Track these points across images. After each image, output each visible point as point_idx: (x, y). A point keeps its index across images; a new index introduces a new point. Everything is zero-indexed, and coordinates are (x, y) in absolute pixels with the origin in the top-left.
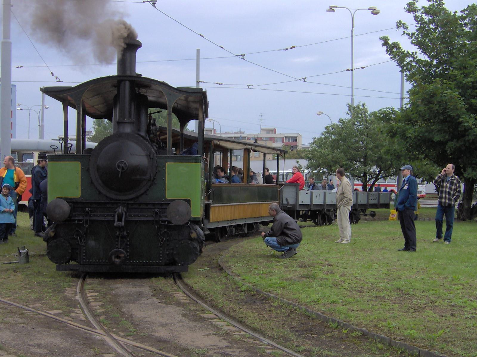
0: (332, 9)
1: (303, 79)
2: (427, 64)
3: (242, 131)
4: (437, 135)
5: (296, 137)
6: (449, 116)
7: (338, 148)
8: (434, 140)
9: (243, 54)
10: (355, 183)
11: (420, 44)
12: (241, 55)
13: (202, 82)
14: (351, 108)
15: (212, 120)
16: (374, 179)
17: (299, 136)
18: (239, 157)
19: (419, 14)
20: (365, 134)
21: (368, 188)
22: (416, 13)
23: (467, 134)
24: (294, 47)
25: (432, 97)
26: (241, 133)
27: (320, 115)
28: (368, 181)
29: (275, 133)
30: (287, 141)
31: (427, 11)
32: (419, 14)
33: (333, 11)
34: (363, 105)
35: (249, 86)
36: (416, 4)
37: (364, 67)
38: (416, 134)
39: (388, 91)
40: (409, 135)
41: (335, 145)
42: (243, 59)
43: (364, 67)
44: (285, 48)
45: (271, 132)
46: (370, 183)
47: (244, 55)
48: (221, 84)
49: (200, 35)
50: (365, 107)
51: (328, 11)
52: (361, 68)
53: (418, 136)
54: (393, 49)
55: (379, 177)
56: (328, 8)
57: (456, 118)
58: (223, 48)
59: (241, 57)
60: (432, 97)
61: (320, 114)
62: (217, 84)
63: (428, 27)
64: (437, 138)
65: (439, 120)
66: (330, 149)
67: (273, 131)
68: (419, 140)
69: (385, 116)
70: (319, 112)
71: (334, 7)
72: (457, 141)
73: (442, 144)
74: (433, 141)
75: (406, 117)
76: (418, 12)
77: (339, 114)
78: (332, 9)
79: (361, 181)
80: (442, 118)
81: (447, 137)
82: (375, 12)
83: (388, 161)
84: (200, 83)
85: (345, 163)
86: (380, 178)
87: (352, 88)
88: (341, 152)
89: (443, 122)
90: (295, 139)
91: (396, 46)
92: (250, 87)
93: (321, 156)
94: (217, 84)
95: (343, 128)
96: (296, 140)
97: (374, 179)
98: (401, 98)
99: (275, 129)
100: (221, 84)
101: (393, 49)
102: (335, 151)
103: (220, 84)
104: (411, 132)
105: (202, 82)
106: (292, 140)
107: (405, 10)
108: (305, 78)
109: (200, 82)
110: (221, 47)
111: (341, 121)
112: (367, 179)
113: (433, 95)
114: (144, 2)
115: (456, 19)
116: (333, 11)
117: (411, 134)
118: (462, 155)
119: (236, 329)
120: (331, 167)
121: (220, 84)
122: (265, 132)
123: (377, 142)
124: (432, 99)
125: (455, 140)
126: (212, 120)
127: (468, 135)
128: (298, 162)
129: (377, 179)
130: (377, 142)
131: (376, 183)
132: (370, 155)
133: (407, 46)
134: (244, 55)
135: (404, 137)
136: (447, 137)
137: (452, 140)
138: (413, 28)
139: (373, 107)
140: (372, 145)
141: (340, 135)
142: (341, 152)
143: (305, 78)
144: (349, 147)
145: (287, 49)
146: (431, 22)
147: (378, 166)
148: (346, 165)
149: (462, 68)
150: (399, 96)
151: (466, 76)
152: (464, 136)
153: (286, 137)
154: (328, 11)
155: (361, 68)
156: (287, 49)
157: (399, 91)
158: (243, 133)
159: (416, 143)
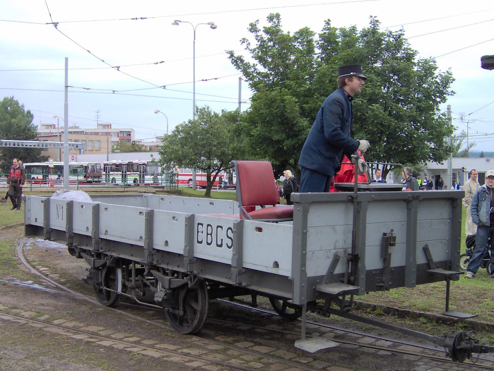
0: (176, 23)
1: (163, 86)
2: (266, 76)
3: (77, 125)
4: (276, 135)
5: (130, 132)
6: (286, 119)
7: (186, 145)
8: (274, 139)
9: (118, 66)
10: (197, 174)
11: (261, 59)
12: (117, 67)
13: (70, 87)
14: (197, 110)
15: (57, 117)
16: (217, 171)
17: (132, 131)
18: (82, 150)
19: (259, 34)
20: (210, 132)
21: (212, 178)
22: (257, 32)
23: (300, 134)
24: (164, 62)
25: (272, 102)
26: (76, 127)
27: (157, 113)
28: (212, 172)
29: (111, 128)
30: (122, 135)
31: (267, 31)
32: (259, 34)
33: (178, 24)
34: (208, 108)
35: (114, 91)
36: (257, 25)
37: (217, 79)
38: (258, 133)
39: (232, 96)
40: (252, 134)
41: (184, 142)
42: (118, 70)
43: (217, 79)
44: (156, 62)
45: (107, 127)
46: (214, 174)
47: (119, 67)
48: (89, 89)
49: (88, 51)
50: (209, 110)
51: (173, 24)
52: (215, 79)
53: (260, 134)
54: (238, 62)
55: (221, 169)
56: (173, 22)
57: (292, 120)
58: (103, 61)
59: (116, 68)
60: (272, 102)
61: (157, 112)
62: (85, 88)
63: (267, 44)
64: (276, 137)
65: (277, 123)
66: (180, 145)
67: (109, 126)
68: (260, 138)
69: (232, 117)
70: (157, 111)
71: (178, 21)
72: (292, 140)
73: (279, 142)
74: (272, 140)
75: (252, 118)
76: (258, 31)
77: (184, 116)
78: (176, 23)
79: (207, 172)
80: (280, 120)
81: (284, 136)
82: (213, 26)
83: (229, 155)
84: (68, 87)
85: (193, 157)
86: (221, 170)
87: (194, 93)
88: (190, 148)
89: (282, 123)
90: (129, 133)
91: (240, 59)
92: (115, 92)
93: (172, 151)
94: (85, 88)
95: (190, 127)
96: (130, 135)
97: (217, 171)
98: (239, 102)
99: (111, 125)
100: (89, 89)
101: (238, 62)
102: (185, 147)
103: (87, 89)
104: (255, 132)
105: (70, 87)
106: (126, 135)
107: (248, 30)
108: (165, 86)
109: (68, 86)
110: (102, 60)
111: (190, 122)
112: (211, 171)
113: (273, 101)
114: (47, 24)
115: (290, 40)
116: (178, 24)
117: (254, 132)
118: (296, 152)
119: (40, 318)
120: (181, 161)
121: (87, 89)
122: (101, 127)
123: (220, 140)
124: (273, 104)
125: (290, 139)
126: (57, 117)
127: (301, 135)
128: (152, 156)
129: (219, 171)
130: (220, 140)
131: (219, 174)
132: (215, 150)
133: (249, 58)
134: (119, 67)
135: (249, 135)
136: (284, 136)
137: (288, 139)
138: (254, 44)
139: (217, 109)
140: (216, 143)
141: (189, 133)
142: (190, 148)
143: (165, 86)
144: (196, 144)
145: (157, 63)
146: (270, 40)
147: (221, 160)
148: (194, 159)
149: (296, 78)
150: (238, 101)
151: (300, 86)
152: (297, 136)
153: (120, 132)
154: (173, 24)
155: (215, 79)
156: (157, 63)
157: (238, 97)
158: (78, 128)
159: (258, 141)
